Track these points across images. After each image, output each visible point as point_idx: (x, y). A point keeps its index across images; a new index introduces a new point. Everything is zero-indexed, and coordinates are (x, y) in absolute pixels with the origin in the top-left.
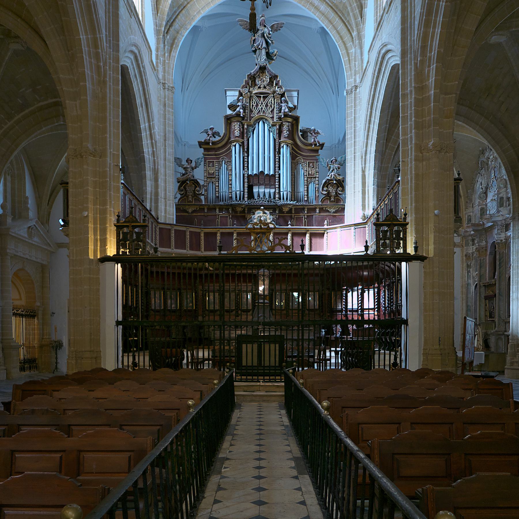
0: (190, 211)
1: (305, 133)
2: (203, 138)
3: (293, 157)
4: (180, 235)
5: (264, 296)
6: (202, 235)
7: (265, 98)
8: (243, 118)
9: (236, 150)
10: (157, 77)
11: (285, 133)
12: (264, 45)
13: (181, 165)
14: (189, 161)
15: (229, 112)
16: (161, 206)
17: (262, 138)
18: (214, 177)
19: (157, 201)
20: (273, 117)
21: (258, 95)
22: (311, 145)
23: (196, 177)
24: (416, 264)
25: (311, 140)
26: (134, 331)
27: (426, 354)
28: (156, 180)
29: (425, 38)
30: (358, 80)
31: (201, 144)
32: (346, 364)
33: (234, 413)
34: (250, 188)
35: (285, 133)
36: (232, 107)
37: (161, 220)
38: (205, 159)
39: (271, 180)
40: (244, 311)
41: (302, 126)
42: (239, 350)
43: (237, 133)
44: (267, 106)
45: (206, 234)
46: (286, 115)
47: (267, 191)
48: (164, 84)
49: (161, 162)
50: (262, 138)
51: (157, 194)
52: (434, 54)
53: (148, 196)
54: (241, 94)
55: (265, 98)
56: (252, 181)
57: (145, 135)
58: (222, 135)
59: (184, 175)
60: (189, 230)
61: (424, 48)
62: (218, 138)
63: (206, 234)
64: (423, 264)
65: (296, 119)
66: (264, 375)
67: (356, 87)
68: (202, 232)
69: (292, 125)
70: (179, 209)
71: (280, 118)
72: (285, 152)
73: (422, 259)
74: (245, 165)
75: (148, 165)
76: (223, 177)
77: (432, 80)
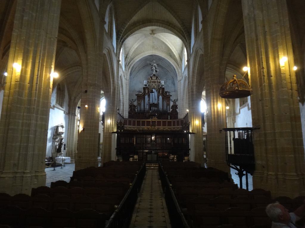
0: (133, 114)
1: (166, 92)
2: (137, 93)
3: (163, 99)
4: (130, 122)
5: (154, 141)
6: (136, 121)
7: (155, 83)
8: (149, 88)
9: (146, 97)
10: (125, 78)
11: (161, 92)
12: (155, 69)
13: (131, 101)
14: (133, 100)
15: (145, 86)
16: (125, 113)
17: (155, 94)
18: (139, 104)
19: (123, 111)
20: (157, 88)
21: (153, 82)
22: (168, 95)
23: (135, 105)
24: (192, 135)
25: (168, 94)
26: (119, 153)
27: (196, 158)
28: (123, 106)
29: (193, 81)
30: (181, 78)
31: (136, 95)
32: (132, 183)
33: (68, 98)
34: (150, 108)
35: (161, 92)
36: (146, 85)
37: (125, 118)
38: (137, 99)
39: (157, 105)
40: (148, 144)
41: (166, 90)
42: (146, 156)
43: (147, 92)
44: (155, 85)
45: (137, 121)
46: (161, 87)
47: (155, 108)
48: (126, 79)
49: (125, 101)
50: (155, 94)
51: (123, 110)
52: (195, 84)
53: (121, 110)
54: (148, 82)
55: (155, 83)
56: (151, 105)
57: (121, 94)
58: (142, 92)
59: (131, 103)
60: (132, 120)
61: (193, 83)
62: (141, 93)
63: (137, 121)
64: (194, 134)
65: (164, 88)
66: (154, 163)
67: (180, 80)
68: (136, 120)
69: (163, 90)
70: (129, 113)
71: (159, 88)
72: (161, 97)
73: (194, 133)
74: (149, 100)
75: (121, 102)
76: (142, 104)
77: (195, 90)
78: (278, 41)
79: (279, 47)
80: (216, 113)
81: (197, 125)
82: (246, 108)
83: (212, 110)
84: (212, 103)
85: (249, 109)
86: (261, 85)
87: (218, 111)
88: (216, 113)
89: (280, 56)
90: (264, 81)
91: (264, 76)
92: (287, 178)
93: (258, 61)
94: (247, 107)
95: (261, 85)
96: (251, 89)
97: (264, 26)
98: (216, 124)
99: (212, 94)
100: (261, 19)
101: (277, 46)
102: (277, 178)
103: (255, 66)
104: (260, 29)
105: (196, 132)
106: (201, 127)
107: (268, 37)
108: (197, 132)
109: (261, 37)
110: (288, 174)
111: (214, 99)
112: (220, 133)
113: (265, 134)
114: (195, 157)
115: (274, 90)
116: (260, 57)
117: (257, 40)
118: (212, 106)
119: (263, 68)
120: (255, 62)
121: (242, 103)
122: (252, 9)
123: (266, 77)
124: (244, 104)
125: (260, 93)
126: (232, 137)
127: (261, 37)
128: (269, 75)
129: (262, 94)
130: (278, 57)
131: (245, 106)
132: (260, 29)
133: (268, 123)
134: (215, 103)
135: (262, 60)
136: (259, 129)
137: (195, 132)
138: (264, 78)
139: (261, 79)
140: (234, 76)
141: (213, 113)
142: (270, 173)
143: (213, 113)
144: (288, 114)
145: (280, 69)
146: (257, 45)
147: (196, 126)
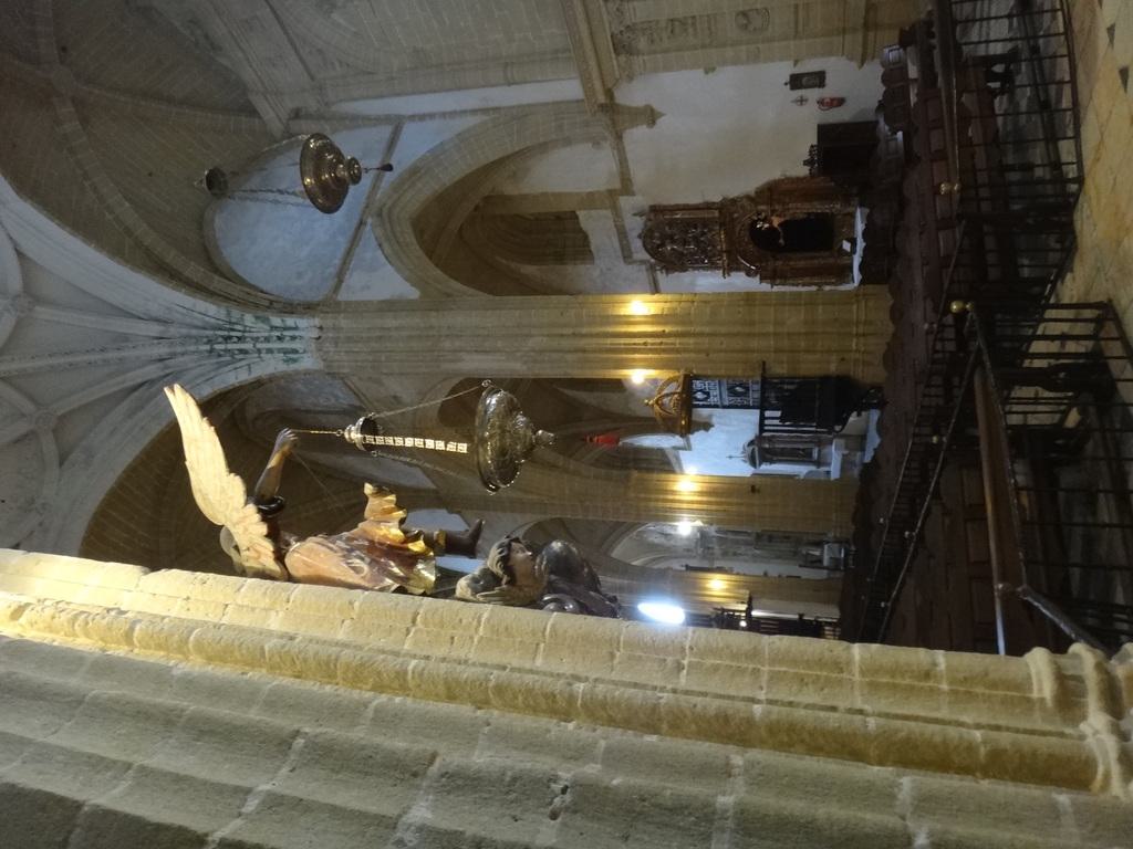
24: (754, 603)
27: (827, 602)
78: (597, 314)
79: (610, 312)
80: (705, 499)
81: (725, 587)
82: (683, 455)
83: (695, 506)
84: (677, 505)
85: (688, 447)
86: (678, 351)
87: (701, 493)
88: (705, 499)
89: (627, 314)
90: (672, 344)
91: (661, 343)
92: (864, 318)
93: (624, 350)
94: (681, 452)
95: (678, 351)
96: (682, 372)
97: (562, 335)
98: (735, 500)
99: (652, 504)
100: (545, 339)
101: (608, 316)
102: (864, 335)
103: (634, 360)
104: (565, 343)
105: (748, 592)
106: (733, 577)
107: (584, 330)
108: (745, 586)
109: (583, 343)
110: (855, 317)
111: (657, 500)
112: (759, 491)
113: (777, 351)
114: (825, 603)
115: (687, 328)
116: (1051, 200)
117: (584, 351)
118: (685, 506)
119: (645, 344)
120: (626, 360)
121: (667, 468)
122: (519, 354)
123: (664, 340)
124: (669, 463)
125: (693, 355)
126: (777, 422)
127: (583, 343)
128: (662, 335)
129: (699, 351)
130: (620, 316)
131: (678, 458)
132: (565, 343)
133: (755, 344)
134: (677, 497)
135: (629, 344)
136: (764, 363)
137: (745, 593)
138: (666, 344)
139: (664, 351)
140: (647, 404)
141: (705, 507)
142: (854, 347)
143: (705, 507)
144: (741, 309)
145: (653, 316)
146: (594, 351)
147: (727, 590)
